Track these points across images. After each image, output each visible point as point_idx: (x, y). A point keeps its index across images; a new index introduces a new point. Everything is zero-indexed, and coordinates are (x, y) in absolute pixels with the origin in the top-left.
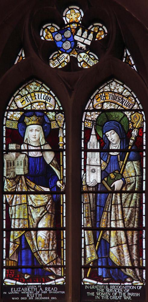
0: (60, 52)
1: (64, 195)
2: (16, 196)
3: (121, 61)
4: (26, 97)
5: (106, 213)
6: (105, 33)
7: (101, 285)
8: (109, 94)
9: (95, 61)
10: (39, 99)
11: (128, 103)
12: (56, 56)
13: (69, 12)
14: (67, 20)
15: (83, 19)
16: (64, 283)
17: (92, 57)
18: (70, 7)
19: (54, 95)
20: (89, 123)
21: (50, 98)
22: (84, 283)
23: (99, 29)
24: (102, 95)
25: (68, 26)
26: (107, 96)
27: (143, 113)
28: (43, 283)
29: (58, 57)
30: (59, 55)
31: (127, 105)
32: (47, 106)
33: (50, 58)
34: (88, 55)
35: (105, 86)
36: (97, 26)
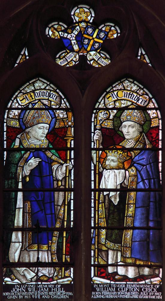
0: (68, 51)
1: (72, 193)
4: (112, 94)
6: (118, 33)
7: (113, 284)
8: (124, 92)
9: (106, 59)
12: (64, 55)
16: (160, 282)
17: (103, 55)
18: (79, 6)
20: (109, 123)
22: (5, 283)
23: (111, 28)
24: (113, 94)
29: (65, 56)
30: (66, 53)
33: (57, 57)
34: (98, 53)
35: (25, 88)
36: (109, 25)
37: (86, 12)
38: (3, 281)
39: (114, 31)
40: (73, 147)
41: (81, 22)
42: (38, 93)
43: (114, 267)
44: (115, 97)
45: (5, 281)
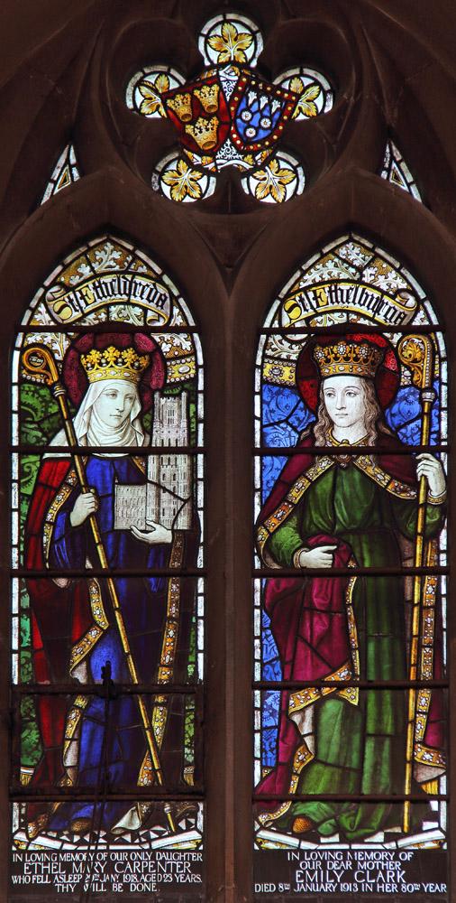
5: (25, 644)
10: (142, 299)
11: (154, 291)
16: (198, 845)
19: (277, 303)
21: (163, 297)
31: (362, 302)
32: (148, 320)
42: (109, 285)
43: (388, 805)
44: (308, 307)
45: (16, 842)
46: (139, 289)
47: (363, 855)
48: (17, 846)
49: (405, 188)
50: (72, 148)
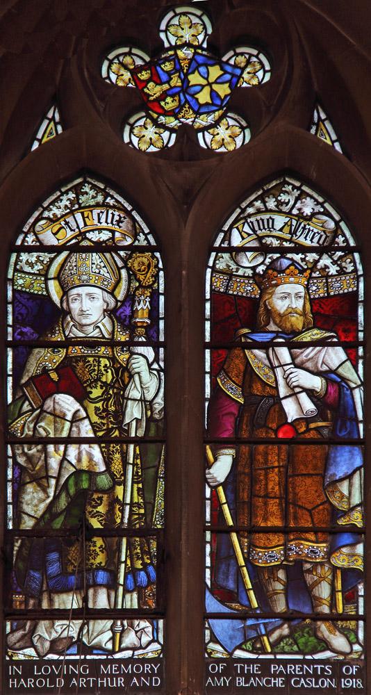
2: (77, 451)
3: (302, 131)
13: (175, 21)
14: (168, 39)
15: (211, 40)
25: (171, 53)
26: (88, 217)
27: (158, 255)
28: (308, 654)
37: (194, 24)
38: (206, 649)
39: (256, 63)
40: (161, 349)
41: (181, 47)
46: (311, 234)
47: (119, 668)
48: (210, 654)
49: (329, 142)
50: (319, 108)
